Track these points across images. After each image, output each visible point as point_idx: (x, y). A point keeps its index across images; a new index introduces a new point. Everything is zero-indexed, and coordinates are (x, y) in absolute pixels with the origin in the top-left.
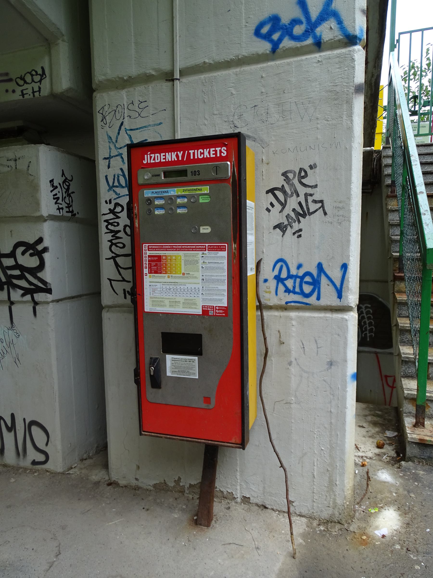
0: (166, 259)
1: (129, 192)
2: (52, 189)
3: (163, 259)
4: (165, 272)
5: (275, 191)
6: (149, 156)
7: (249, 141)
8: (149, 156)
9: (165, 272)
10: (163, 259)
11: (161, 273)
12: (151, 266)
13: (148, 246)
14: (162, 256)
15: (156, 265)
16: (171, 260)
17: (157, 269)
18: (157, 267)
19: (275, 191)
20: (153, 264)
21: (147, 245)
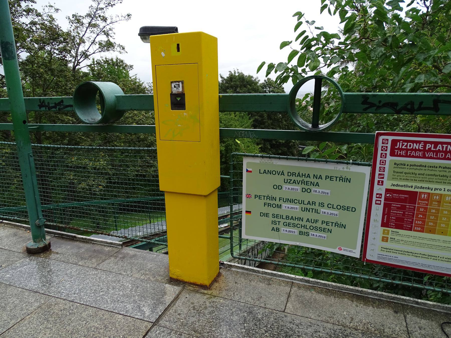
0: (428, 200)
1: (174, 94)
2: (3, 41)
3: (420, 199)
4: (419, 229)
5: (400, 3)
6: (401, 143)
7: (273, 80)
8: (401, 143)
9: (419, 229)
10: (420, 199)
11: (410, 229)
12: (389, 210)
13: (394, 142)
14: (420, 193)
15: (403, 208)
16: (439, 202)
17: (404, 214)
18: (404, 212)
19: (400, 3)
20: (395, 205)
21: (390, 138)
